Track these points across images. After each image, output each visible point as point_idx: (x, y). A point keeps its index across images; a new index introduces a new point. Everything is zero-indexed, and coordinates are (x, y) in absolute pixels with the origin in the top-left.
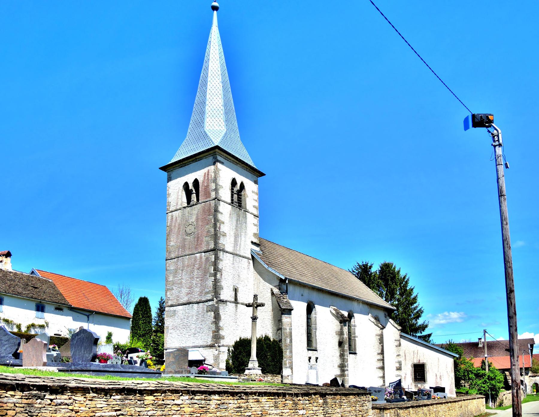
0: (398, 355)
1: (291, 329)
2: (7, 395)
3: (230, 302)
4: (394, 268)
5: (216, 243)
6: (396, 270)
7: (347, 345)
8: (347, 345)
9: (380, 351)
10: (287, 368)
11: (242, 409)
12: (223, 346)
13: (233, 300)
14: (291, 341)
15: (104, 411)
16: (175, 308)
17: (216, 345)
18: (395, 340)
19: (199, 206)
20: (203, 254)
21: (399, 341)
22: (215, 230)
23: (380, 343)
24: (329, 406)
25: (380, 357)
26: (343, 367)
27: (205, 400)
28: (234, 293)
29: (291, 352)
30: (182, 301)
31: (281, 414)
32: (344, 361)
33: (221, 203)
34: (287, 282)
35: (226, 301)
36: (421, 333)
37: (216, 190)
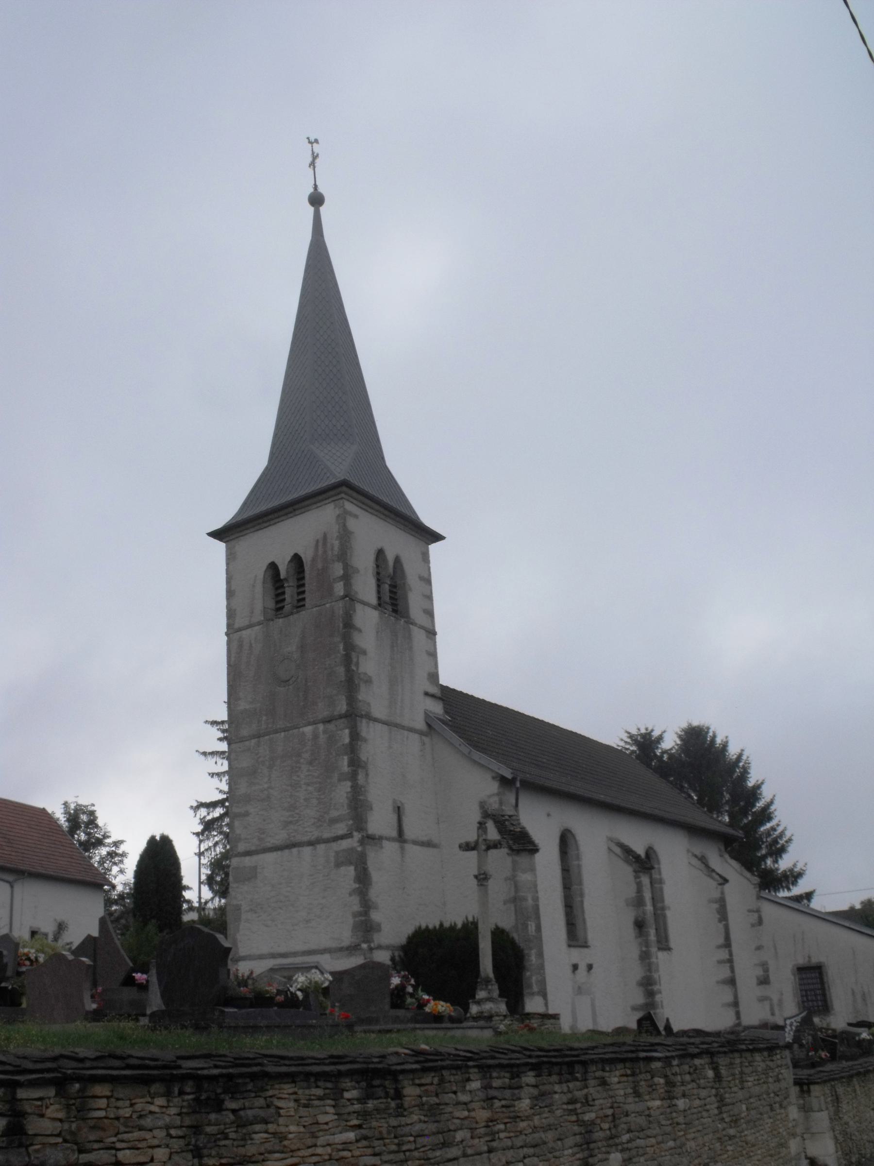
0: (759, 948)
1: (536, 899)
2: (153, 1108)
3: (388, 839)
4: (714, 736)
5: (352, 700)
6: (719, 740)
7: (649, 928)
8: (649, 928)
9: (721, 941)
10: (533, 994)
11: (578, 1106)
12: (380, 947)
13: (394, 834)
14: (539, 928)
15: (332, 1130)
16: (255, 858)
17: (364, 946)
18: (749, 911)
19: (304, 615)
20: (321, 727)
21: (758, 911)
22: (348, 670)
23: (720, 921)
24: (724, 1084)
25: (723, 954)
26: (648, 985)
27: (510, 1088)
28: (395, 817)
29: (540, 955)
30: (271, 842)
31: (647, 1113)
32: (650, 970)
33: (359, 607)
34: (518, 784)
35: (381, 838)
36: (789, 889)
37: (347, 578)
